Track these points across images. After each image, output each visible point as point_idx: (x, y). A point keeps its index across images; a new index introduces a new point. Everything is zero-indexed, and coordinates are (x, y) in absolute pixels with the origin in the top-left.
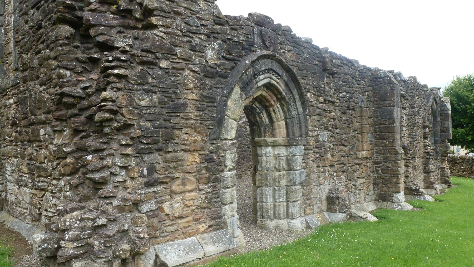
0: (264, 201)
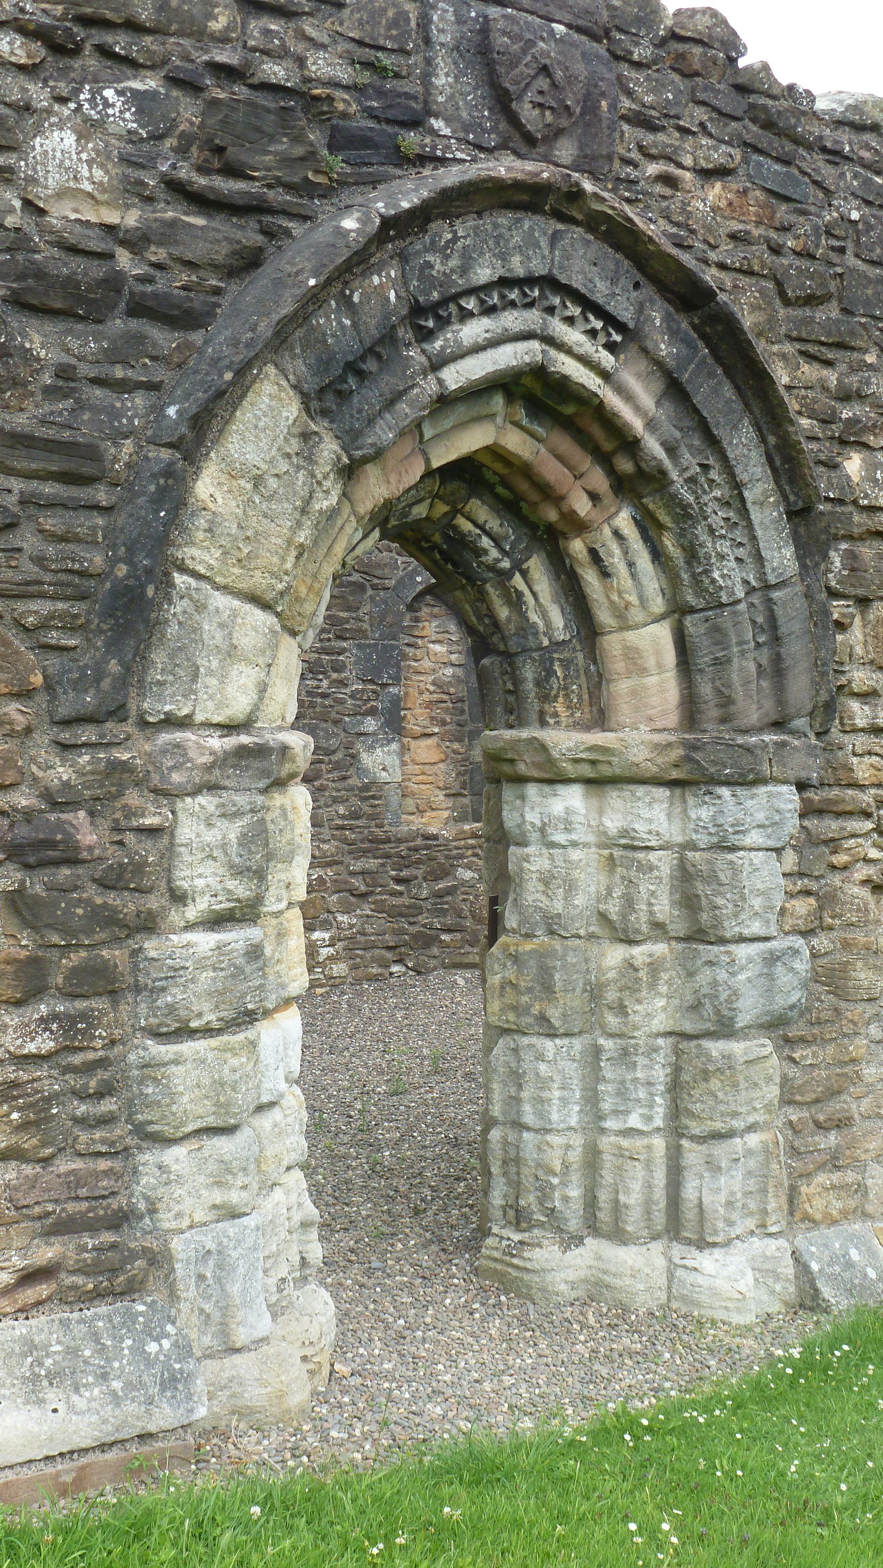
0: (529, 1118)
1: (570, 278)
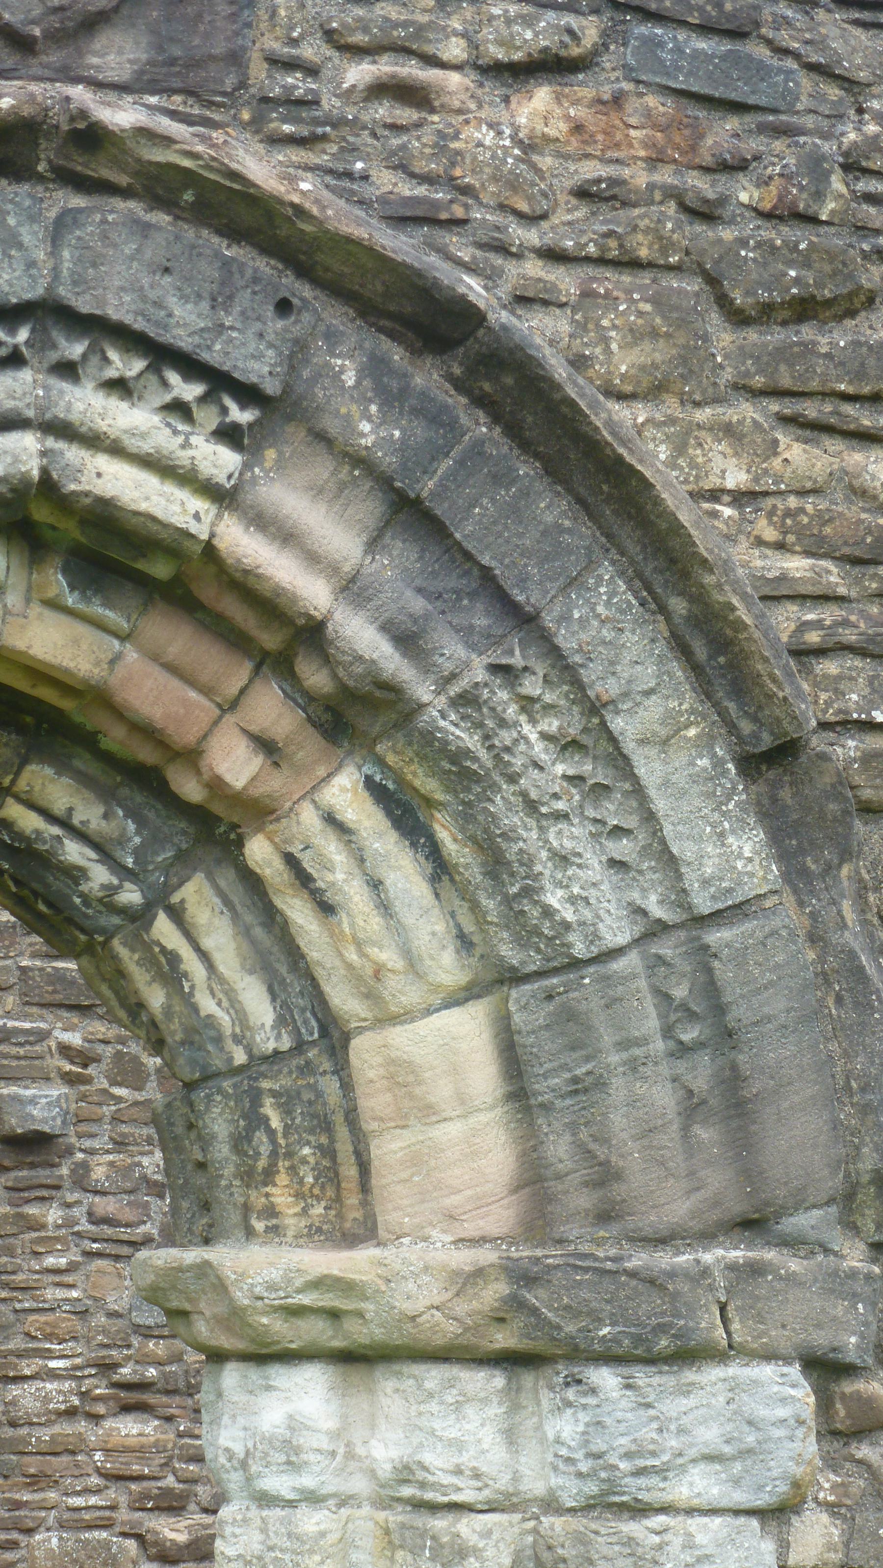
1: (101, 302)
